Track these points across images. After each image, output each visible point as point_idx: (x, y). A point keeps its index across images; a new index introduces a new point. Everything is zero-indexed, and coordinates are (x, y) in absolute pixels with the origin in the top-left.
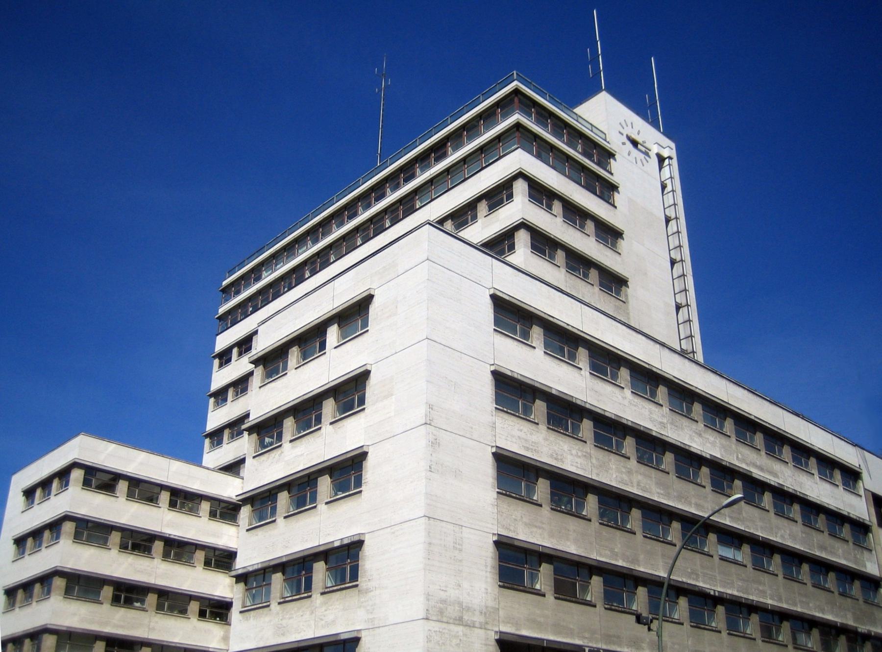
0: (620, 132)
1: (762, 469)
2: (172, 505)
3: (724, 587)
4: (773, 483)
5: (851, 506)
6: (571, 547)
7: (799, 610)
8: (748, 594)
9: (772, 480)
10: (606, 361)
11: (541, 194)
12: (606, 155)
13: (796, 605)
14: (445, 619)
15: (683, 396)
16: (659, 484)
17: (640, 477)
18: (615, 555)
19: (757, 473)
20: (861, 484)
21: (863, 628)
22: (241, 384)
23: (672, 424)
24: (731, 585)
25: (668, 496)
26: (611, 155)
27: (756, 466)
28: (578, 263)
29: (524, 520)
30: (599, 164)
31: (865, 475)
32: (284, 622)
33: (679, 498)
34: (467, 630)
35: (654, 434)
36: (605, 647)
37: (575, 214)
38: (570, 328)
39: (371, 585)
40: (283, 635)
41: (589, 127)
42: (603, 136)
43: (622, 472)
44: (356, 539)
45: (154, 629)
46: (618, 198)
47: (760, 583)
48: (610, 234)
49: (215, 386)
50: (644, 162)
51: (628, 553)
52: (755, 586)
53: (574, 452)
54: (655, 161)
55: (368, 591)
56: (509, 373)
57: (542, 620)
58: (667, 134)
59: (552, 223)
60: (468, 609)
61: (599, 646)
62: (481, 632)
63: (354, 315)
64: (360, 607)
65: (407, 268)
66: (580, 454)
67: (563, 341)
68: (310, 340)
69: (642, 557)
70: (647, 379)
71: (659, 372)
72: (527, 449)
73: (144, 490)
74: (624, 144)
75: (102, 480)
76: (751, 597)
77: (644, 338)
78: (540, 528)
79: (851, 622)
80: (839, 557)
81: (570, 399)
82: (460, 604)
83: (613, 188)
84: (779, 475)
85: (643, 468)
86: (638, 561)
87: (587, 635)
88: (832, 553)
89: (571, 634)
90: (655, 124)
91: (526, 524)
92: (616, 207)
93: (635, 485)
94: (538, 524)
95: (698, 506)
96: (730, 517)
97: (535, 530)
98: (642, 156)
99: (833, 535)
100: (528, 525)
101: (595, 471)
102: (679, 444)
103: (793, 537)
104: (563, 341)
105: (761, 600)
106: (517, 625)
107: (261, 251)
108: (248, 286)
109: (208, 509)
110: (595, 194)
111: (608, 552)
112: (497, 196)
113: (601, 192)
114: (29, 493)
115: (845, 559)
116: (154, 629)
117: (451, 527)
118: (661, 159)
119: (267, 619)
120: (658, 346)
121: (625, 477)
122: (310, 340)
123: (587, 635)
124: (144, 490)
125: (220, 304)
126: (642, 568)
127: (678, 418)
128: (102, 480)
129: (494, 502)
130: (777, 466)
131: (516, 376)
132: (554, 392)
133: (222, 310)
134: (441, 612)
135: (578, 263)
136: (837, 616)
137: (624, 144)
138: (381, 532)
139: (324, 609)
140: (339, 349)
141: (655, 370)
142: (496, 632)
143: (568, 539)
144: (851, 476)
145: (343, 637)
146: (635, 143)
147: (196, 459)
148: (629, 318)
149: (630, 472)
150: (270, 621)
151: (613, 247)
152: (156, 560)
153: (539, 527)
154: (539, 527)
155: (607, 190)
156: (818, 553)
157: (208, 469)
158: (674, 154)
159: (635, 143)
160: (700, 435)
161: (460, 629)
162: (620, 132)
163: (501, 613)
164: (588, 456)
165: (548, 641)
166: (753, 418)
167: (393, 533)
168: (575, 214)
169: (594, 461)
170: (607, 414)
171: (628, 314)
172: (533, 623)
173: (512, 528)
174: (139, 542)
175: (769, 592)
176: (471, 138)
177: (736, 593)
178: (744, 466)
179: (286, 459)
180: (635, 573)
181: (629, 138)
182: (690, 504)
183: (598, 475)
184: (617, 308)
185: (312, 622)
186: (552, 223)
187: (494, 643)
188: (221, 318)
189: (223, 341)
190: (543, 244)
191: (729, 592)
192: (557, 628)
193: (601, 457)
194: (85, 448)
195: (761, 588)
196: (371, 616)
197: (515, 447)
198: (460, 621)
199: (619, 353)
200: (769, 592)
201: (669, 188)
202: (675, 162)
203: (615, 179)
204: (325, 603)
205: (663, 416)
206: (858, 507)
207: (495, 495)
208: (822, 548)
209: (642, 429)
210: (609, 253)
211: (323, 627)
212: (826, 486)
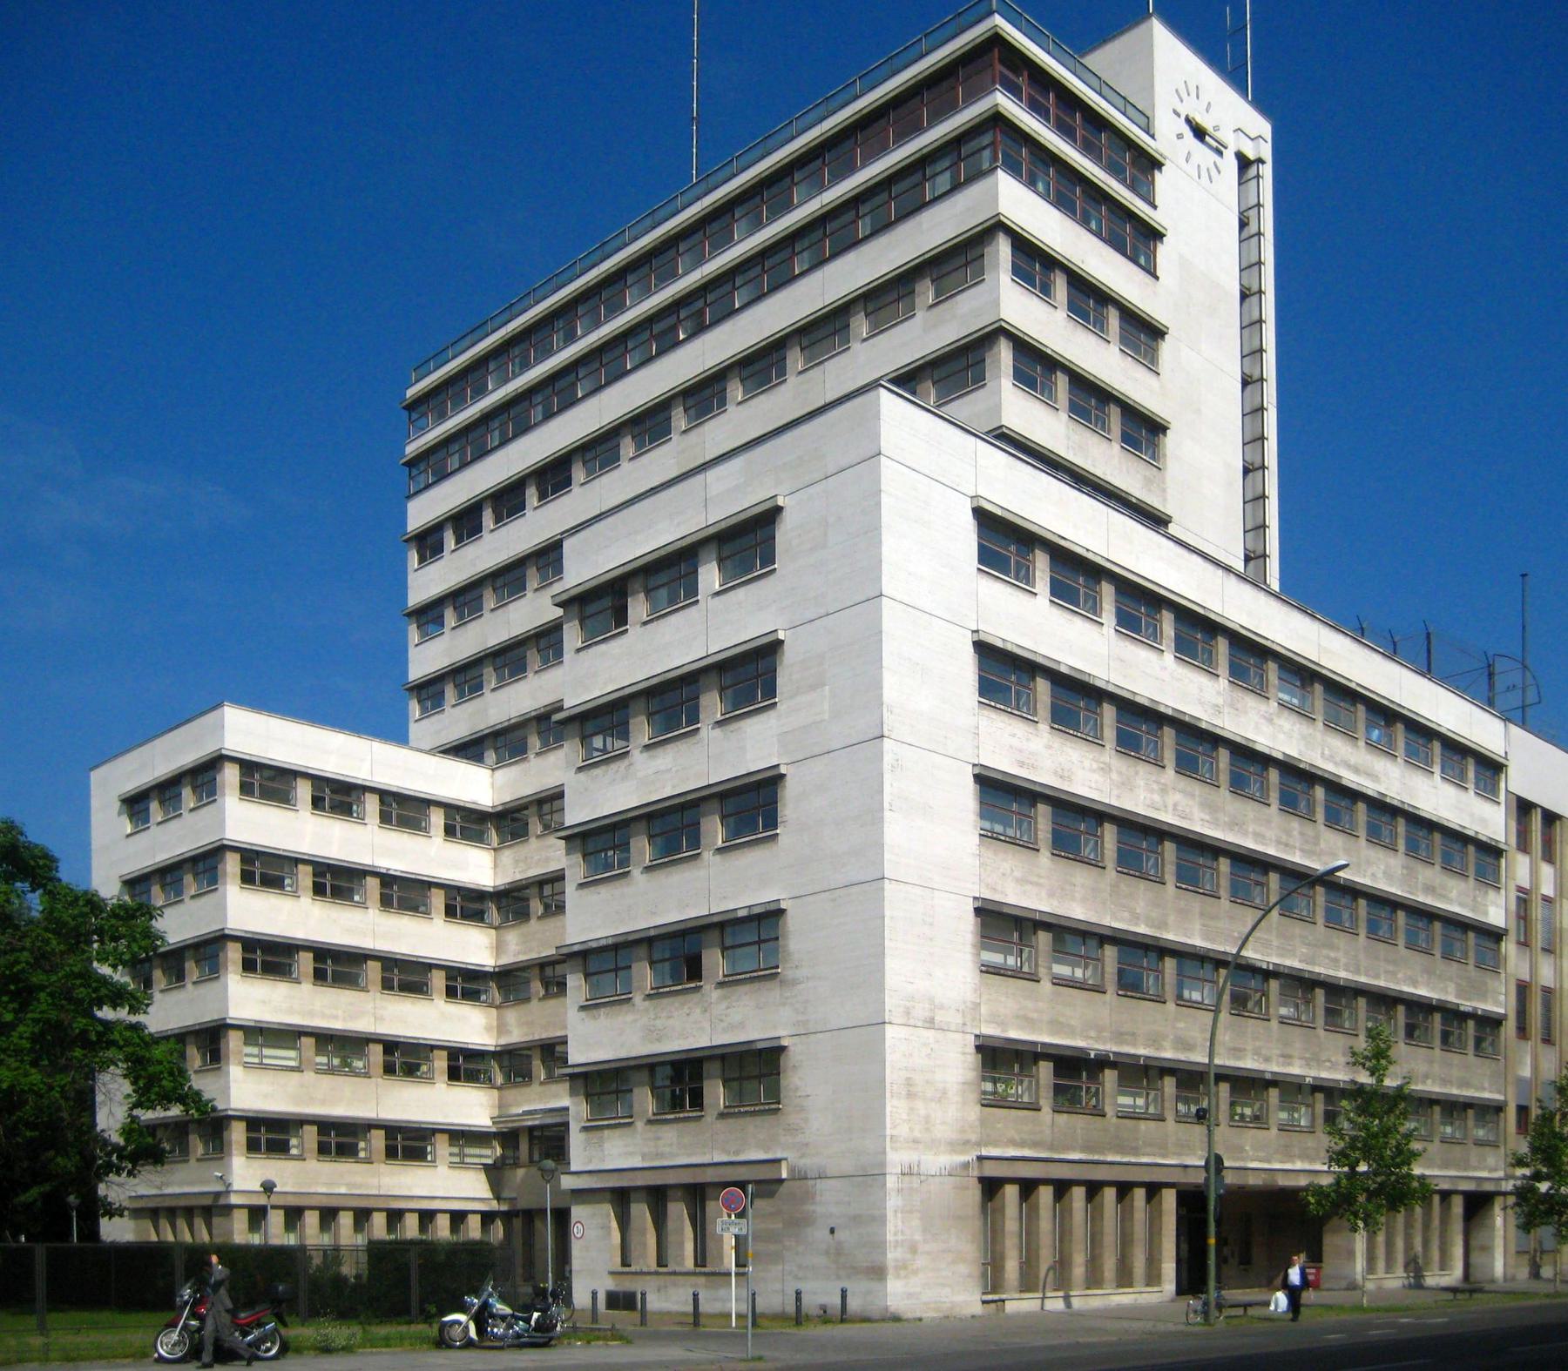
0: (1175, 112)
1: (1357, 770)
2: (385, 818)
3: (1282, 956)
4: (1370, 793)
5: (1483, 821)
6: (1078, 911)
7: (1382, 983)
8: (1314, 964)
9: (1370, 787)
10: (1141, 606)
11: (1036, 264)
12: (1144, 165)
13: (1377, 976)
14: (912, 1022)
15: (1251, 657)
16: (1206, 805)
17: (1178, 797)
18: (1136, 918)
19: (1350, 779)
20: (1503, 785)
21: (1466, 1005)
22: (546, 641)
23: (1232, 706)
24: (1291, 953)
25: (1215, 823)
26: (1155, 164)
27: (1348, 766)
28: (1092, 399)
29: (1016, 874)
30: (1133, 188)
31: (1512, 771)
32: (658, 1023)
33: (1234, 824)
34: (939, 1035)
35: (1204, 726)
36: (1115, 1049)
37: (1089, 299)
38: (1090, 556)
39: (799, 974)
40: (658, 1040)
41: (1120, 103)
42: (1142, 121)
43: (1152, 791)
44: (773, 907)
45: (382, 1019)
46: (1165, 253)
47: (1332, 947)
48: (1143, 334)
49: (416, 598)
50: (1214, 172)
51: (1154, 915)
52: (1325, 952)
53: (1087, 763)
54: (1230, 165)
55: (795, 982)
56: (1000, 644)
57: (1035, 1016)
58: (1262, 104)
59: (1044, 321)
60: (942, 1007)
61: (1108, 1047)
62: (958, 1036)
63: (748, 542)
64: (784, 1004)
65: (844, 463)
66: (1095, 766)
67: (1078, 578)
68: (668, 575)
69: (1171, 919)
70: (1198, 633)
71: (1218, 619)
72: (1022, 764)
73: (338, 797)
74: (1180, 136)
75: (270, 782)
76: (1317, 970)
77: (1199, 560)
78: (1037, 884)
79: (1451, 998)
80: (1450, 901)
81: (1086, 679)
82: (931, 1000)
83: (1153, 235)
84: (1383, 778)
85: (1184, 783)
86: (1166, 924)
87: (1093, 1034)
88: (1443, 897)
89: (1072, 1032)
90: (1234, 76)
91: (1018, 881)
92: (1157, 278)
93: (1170, 808)
94: (1035, 879)
95: (1258, 836)
96: (1302, 850)
97: (1028, 887)
98: (1213, 156)
99: (1447, 867)
100: (1021, 881)
101: (1115, 792)
102: (1238, 740)
103: (1388, 876)
104: (1078, 578)
105: (1332, 973)
106: (1003, 1024)
107: (479, 330)
108: (460, 403)
109: (442, 823)
110: (1124, 254)
111: (1126, 914)
112: (956, 263)
113: (1135, 248)
114: (135, 804)
115: (1461, 905)
116: (382, 1019)
117: (918, 891)
118: (1244, 163)
119: (629, 1018)
120: (1220, 572)
121: (1156, 797)
122: (668, 575)
123: (1093, 1034)
124: (338, 797)
125: (407, 438)
126: (1171, 936)
127: (1239, 694)
128: (270, 782)
129: (975, 850)
130: (1381, 764)
131: (1009, 647)
132: (1063, 669)
133: (411, 449)
134: (908, 1013)
135: (1092, 399)
136: (1433, 989)
137: (1180, 136)
138: (810, 898)
139: (724, 1005)
140: (723, 598)
141: (1213, 616)
142: (977, 1036)
143: (1073, 899)
144: (1491, 768)
145: (760, 1046)
146: (1199, 133)
147: (397, 734)
148: (1165, 500)
149: (1164, 790)
150: (636, 1021)
151: (1149, 360)
152: (370, 911)
153: (1038, 884)
154: (1038, 884)
155: (1138, 238)
156: (1421, 899)
157: (418, 750)
158: (1266, 152)
159: (1199, 133)
160: (1270, 721)
161: (930, 1035)
162: (1175, 112)
163: (983, 1009)
164: (1106, 769)
165: (1044, 1044)
166: (1353, 686)
167: (834, 900)
168: (1089, 299)
169: (1114, 776)
170: (1138, 699)
171: (1164, 490)
172: (1027, 1021)
173: (999, 888)
174: (336, 881)
175: (1343, 960)
176: (903, 136)
177: (1296, 964)
178: (1330, 767)
179: (640, 775)
180: (1162, 944)
181: (1188, 121)
182: (1245, 834)
183: (1118, 797)
184: (1148, 482)
185: (707, 1025)
186: (1044, 321)
187: (972, 1050)
188: (412, 463)
189: (423, 511)
190: (1037, 366)
191: (1288, 963)
192: (1056, 1026)
193: (1124, 769)
194: (248, 732)
195: (1332, 955)
196: (800, 1018)
197: (1004, 763)
198: (930, 1023)
199: (1162, 592)
200: (1343, 960)
201: (1253, 228)
202: (1267, 171)
203: (1157, 217)
204: (725, 998)
205: (1219, 693)
206: (1487, 819)
207: (977, 839)
208: (1430, 889)
209: (1187, 719)
210: (1140, 373)
211: (724, 1030)
212: (1450, 791)
